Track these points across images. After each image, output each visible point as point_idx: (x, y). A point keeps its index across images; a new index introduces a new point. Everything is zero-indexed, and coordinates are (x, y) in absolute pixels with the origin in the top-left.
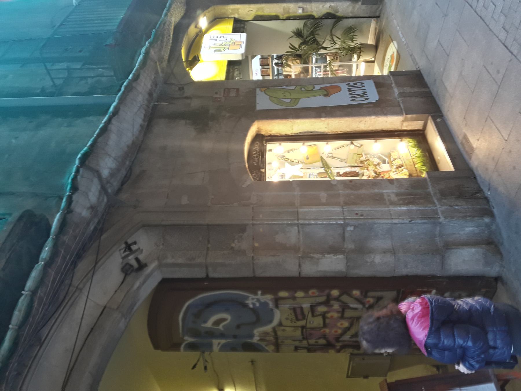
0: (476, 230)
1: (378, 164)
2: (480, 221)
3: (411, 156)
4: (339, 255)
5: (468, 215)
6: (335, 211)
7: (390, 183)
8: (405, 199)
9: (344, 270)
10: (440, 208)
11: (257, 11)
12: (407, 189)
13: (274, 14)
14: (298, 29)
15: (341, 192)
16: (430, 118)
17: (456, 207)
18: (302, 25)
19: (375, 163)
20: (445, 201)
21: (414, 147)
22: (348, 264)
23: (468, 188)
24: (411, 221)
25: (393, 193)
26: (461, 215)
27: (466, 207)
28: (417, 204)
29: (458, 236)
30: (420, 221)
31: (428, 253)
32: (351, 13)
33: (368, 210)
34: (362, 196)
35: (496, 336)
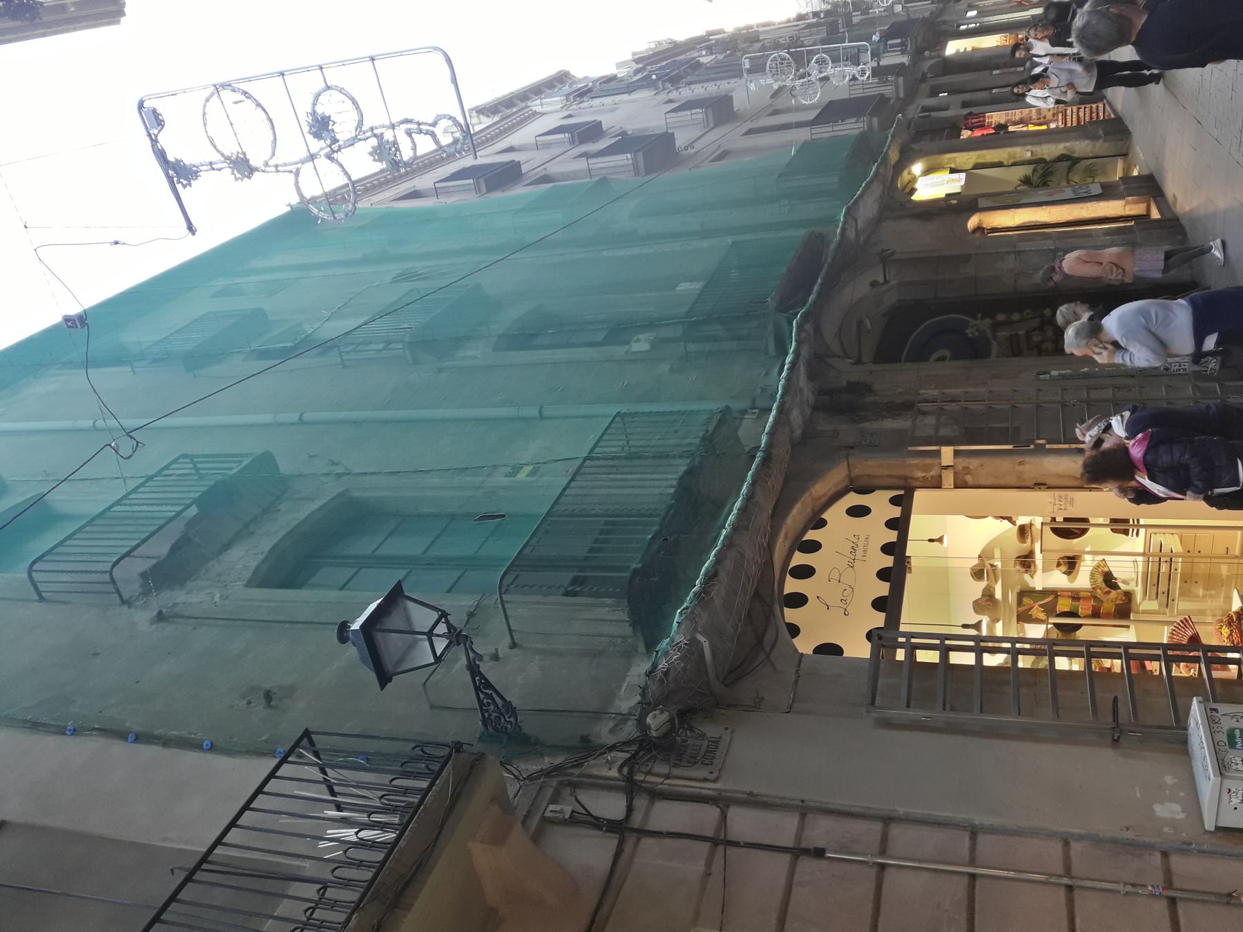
11: (977, 158)
13: (997, 160)
14: (1026, 176)
16: (1151, 199)
18: (1031, 171)
32: (1091, 152)
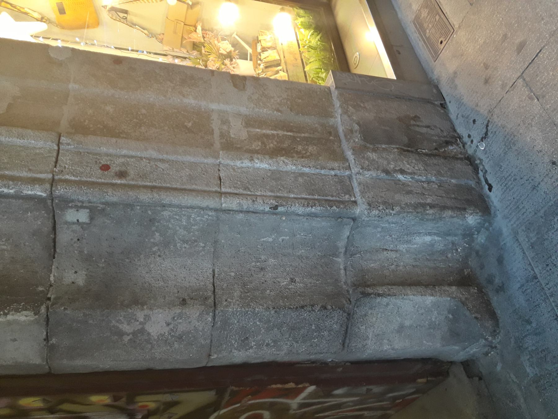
0: (440, 243)
1: (229, 56)
2: (455, 220)
3: (299, 48)
4: (17, 310)
5: (429, 201)
6: (25, 148)
7: (235, 86)
8: (267, 136)
9: (36, 360)
10: (359, 173)
12: (278, 110)
15: (71, 86)
17: (400, 177)
19: (222, 51)
20: (373, 156)
21: (307, 26)
22: (54, 341)
23: (428, 127)
24: (276, 207)
25: (239, 115)
26: (412, 200)
27: (424, 178)
28: (301, 155)
29: (393, 255)
30: (301, 210)
31: (313, 306)
33: (150, 159)
34: (144, 111)
35: (298, 153)
